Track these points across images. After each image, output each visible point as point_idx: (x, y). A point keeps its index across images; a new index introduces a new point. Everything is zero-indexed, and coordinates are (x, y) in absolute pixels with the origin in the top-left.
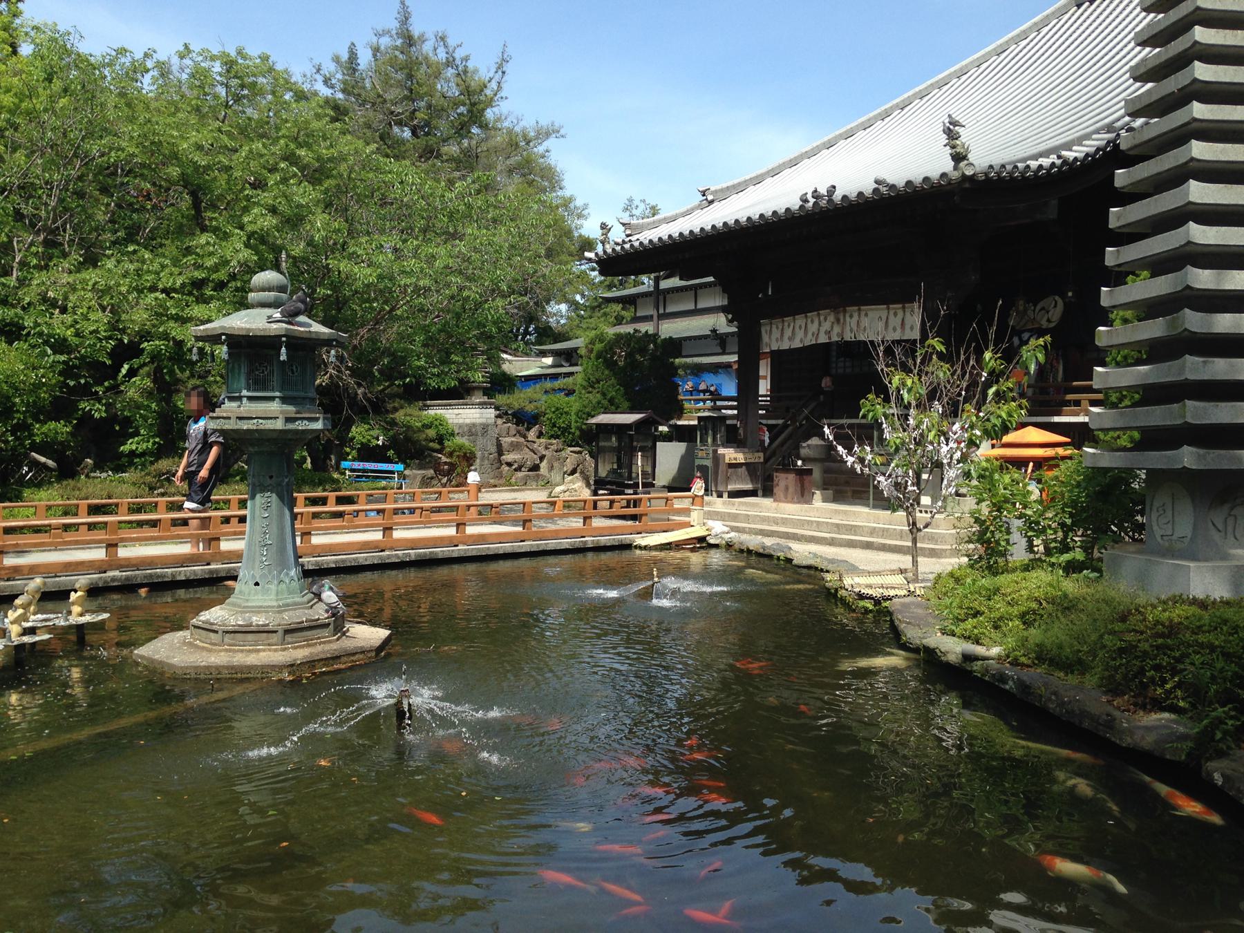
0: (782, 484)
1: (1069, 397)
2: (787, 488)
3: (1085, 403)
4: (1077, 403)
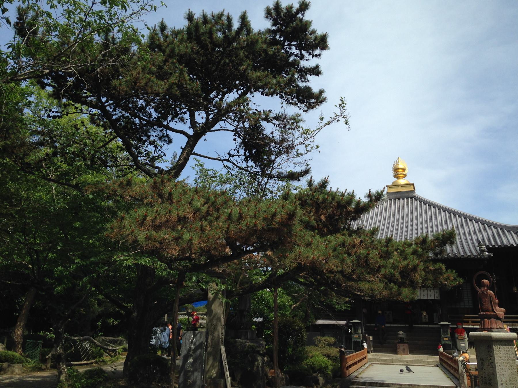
0: (402, 348)
1: (465, 319)
2: (404, 350)
3: (470, 322)
4: (468, 322)
